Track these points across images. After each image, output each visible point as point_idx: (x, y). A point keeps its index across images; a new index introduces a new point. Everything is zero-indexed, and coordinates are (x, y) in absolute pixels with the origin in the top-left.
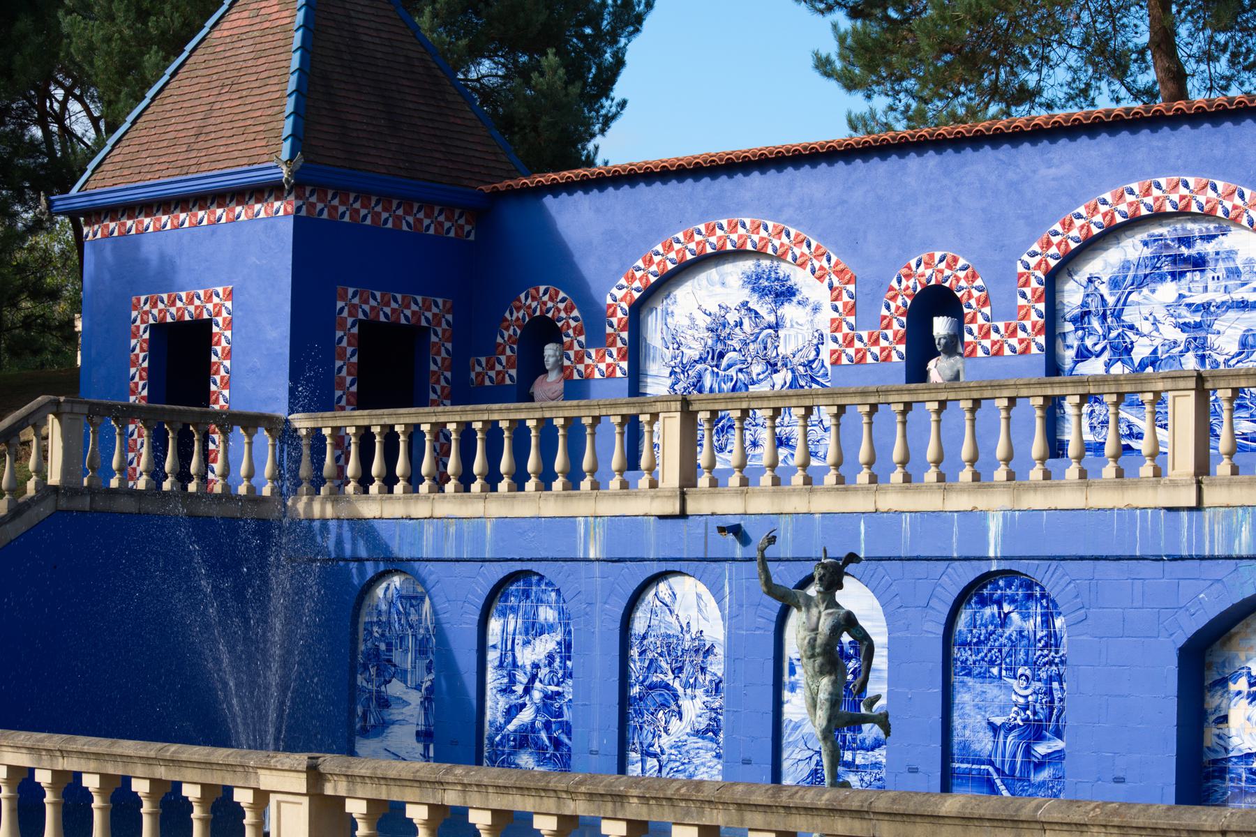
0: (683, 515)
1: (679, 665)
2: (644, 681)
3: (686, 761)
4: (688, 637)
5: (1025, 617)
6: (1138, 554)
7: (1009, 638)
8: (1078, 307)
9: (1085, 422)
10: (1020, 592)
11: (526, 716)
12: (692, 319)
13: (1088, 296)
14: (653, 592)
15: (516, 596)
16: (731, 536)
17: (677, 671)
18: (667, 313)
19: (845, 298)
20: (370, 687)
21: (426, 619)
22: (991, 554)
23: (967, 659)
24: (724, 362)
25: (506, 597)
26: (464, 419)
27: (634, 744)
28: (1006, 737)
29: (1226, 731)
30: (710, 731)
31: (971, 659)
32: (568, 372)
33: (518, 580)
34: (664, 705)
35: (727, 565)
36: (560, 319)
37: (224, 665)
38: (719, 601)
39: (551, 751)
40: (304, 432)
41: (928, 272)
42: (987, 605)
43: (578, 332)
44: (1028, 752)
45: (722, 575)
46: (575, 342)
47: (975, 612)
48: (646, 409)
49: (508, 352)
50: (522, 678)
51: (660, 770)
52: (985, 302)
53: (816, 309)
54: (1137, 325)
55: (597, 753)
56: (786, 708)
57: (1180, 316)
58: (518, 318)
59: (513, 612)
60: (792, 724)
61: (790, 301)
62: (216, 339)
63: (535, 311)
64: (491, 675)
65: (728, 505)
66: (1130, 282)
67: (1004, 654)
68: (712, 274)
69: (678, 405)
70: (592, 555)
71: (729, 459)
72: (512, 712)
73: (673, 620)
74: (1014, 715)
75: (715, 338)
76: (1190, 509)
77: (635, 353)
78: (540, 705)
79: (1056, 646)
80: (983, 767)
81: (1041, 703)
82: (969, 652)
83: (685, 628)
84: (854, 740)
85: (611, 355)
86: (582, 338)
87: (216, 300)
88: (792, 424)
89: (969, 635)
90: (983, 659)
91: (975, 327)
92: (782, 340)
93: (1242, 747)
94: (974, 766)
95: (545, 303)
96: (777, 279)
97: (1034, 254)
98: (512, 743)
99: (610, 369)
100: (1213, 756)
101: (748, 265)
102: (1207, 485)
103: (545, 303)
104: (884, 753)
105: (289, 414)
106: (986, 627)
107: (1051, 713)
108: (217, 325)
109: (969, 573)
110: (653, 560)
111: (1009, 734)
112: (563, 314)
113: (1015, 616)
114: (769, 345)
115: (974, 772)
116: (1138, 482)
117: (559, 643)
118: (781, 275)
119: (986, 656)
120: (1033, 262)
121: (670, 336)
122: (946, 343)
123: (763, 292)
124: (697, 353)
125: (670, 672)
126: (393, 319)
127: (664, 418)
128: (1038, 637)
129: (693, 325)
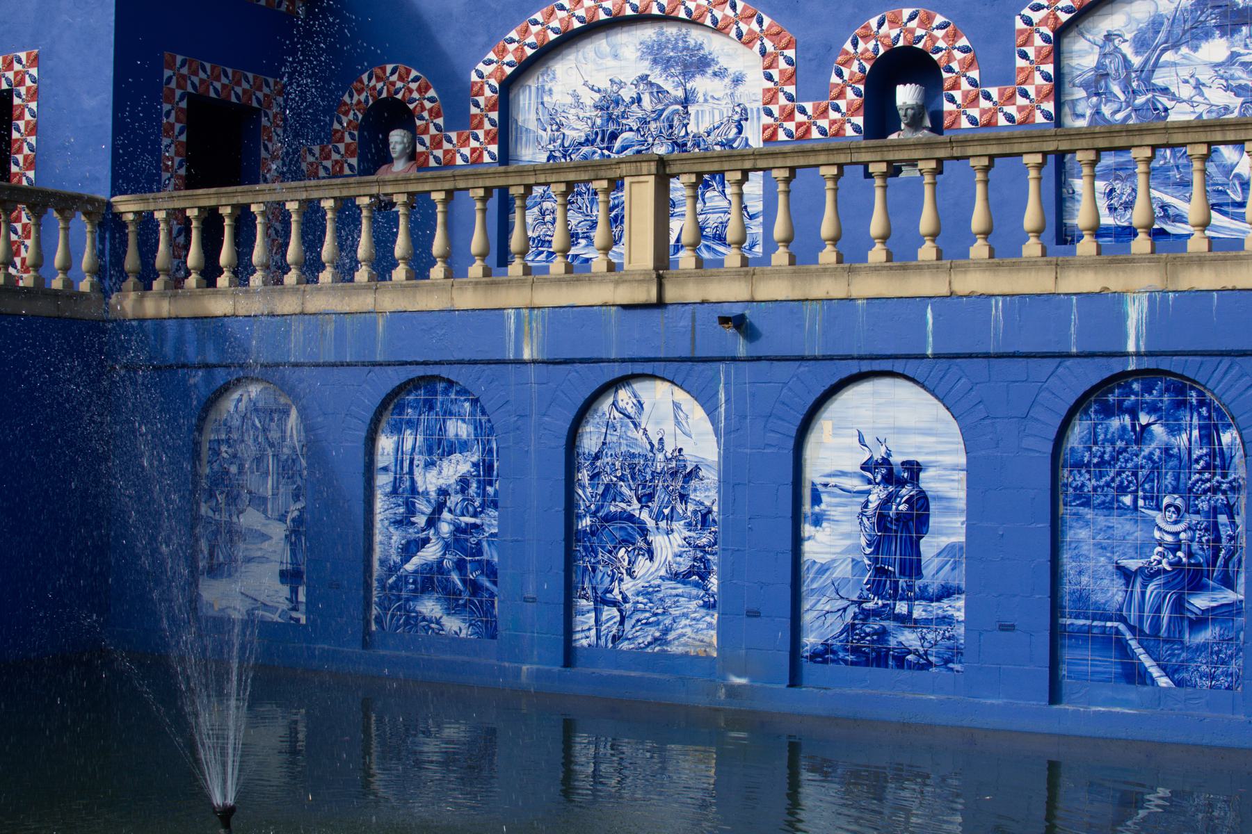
0: (660, 304)
1: (648, 491)
2: (597, 511)
3: (660, 611)
4: (660, 456)
5: (1174, 430)
7: (1149, 458)
8: (1092, 69)
9: (1102, 204)
10: (1166, 398)
11: (431, 553)
12: (576, 96)
13: (1105, 55)
14: (611, 400)
15: (414, 408)
16: (731, 331)
17: (646, 499)
18: (541, 90)
19: (782, 64)
20: (217, 517)
21: (291, 436)
22: (1131, 347)
23: (1083, 485)
24: (618, 144)
25: (400, 409)
26: (345, 193)
27: (583, 589)
28: (1144, 586)
30: (697, 573)
31: (1090, 485)
32: (422, 159)
33: (417, 388)
34: (627, 541)
35: (722, 366)
36: (413, 101)
38: (711, 412)
39: (466, 596)
40: (130, 217)
41: (855, 67)
42: (1113, 415)
43: (435, 113)
45: (714, 380)
46: (431, 125)
47: (1096, 425)
48: (602, 174)
49: (348, 139)
50: (424, 507)
51: (622, 622)
53: (737, 81)
54: (1173, 89)
55: (534, 600)
56: (807, 547)
57: (1232, 77)
58: (359, 102)
59: (410, 427)
60: (816, 567)
61: (703, 73)
62: (17, 113)
63: (380, 92)
64: (380, 504)
65: (729, 292)
66: (1163, 39)
67: (1141, 479)
68: (600, 44)
69: (653, 167)
70: (527, 356)
72: (410, 549)
73: (639, 435)
74: (1158, 558)
75: (606, 117)
77: (505, 134)
78: (450, 540)
79: (1223, 468)
80: (1109, 624)
81: (1200, 542)
82: (1087, 476)
83: (656, 446)
84: (910, 588)
85: (477, 138)
86: (440, 121)
87: (17, 67)
89: (1087, 454)
90: (1108, 485)
91: (957, 95)
92: (692, 117)
94: (1095, 623)
95: (393, 84)
96: (686, 48)
97: (490, 62)
98: (411, 586)
99: (475, 155)
101: (648, 33)
103: (393, 84)
104: (961, 603)
105: (113, 196)
106: (1113, 443)
107: (1216, 556)
108: (19, 96)
109: (1093, 373)
110: (614, 361)
111: (1150, 581)
112: (416, 95)
113: (1158, 429)
114: (676, 123)
115: (1095, 631)
116: (592, 279)
117: (475, 465)
118: (692, 43)
119: (1113, 480)
121: (547, 117)
122: (914, 115)
123: (667, 64)
124: (583, 134)
125: (635, 501)
126: (223, 96)
127: (631, 183)
128: (1194, 456)
129: (579, 104)
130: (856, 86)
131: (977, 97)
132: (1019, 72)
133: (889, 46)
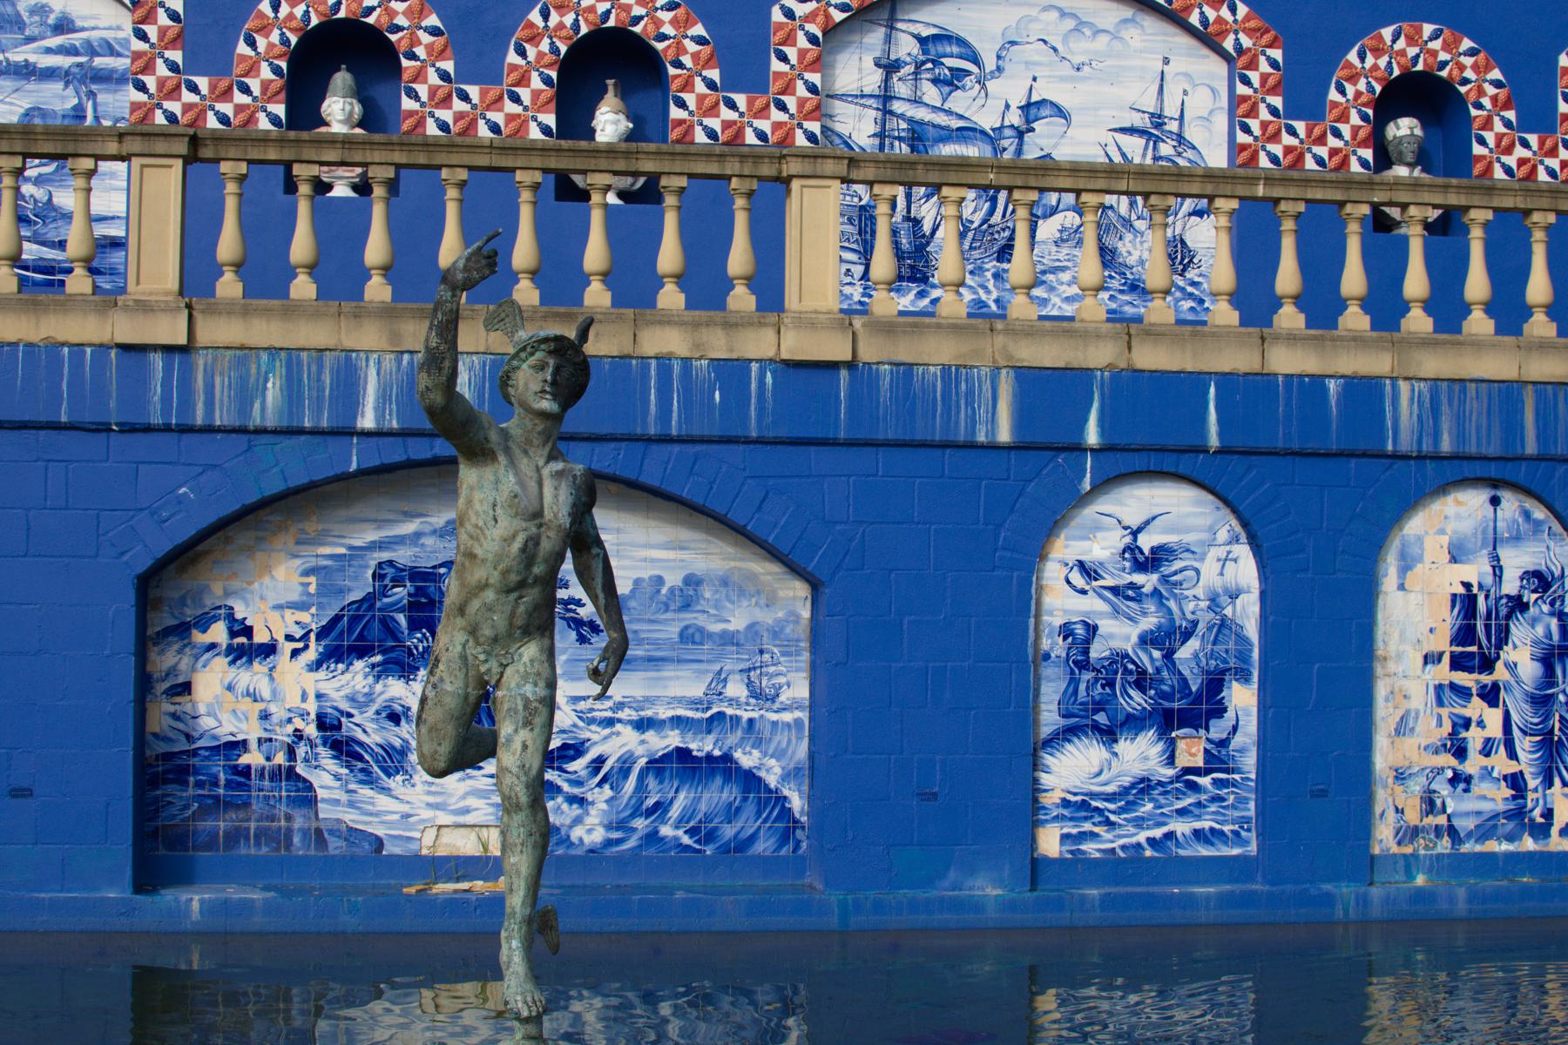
6: (64, 419)
29: (188, 708)
37: (780, 614)
76: (169, 349)
93: (218, 731)
100: (163, 748)
102: (203, 312)
116: (71, 304)
130: (276, 62)
131: (178, 87)
132: (775, 80)
133: (325, 15)
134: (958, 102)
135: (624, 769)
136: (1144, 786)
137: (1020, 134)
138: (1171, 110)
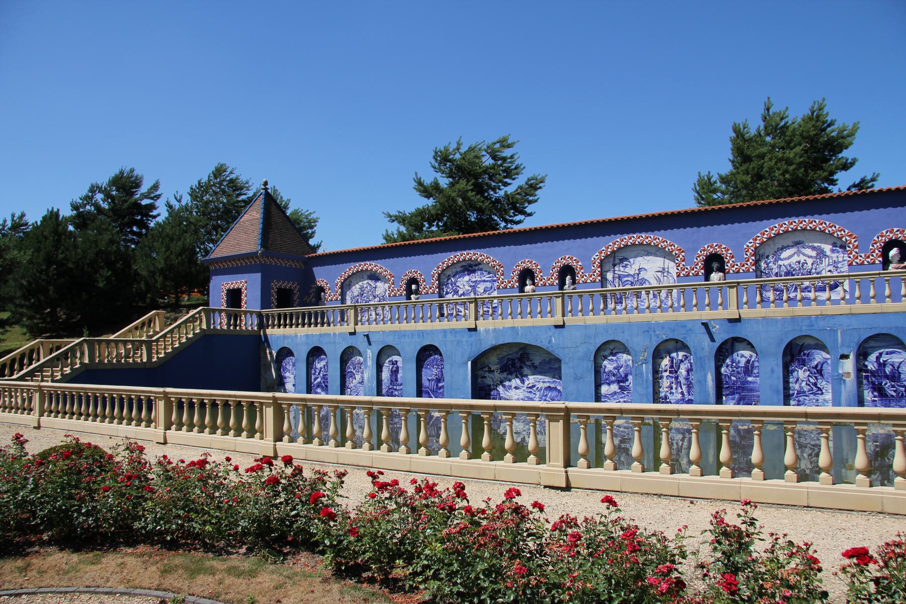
11: (319, 380)
17: (354, 369)
44: (437, 385)
50: (318, 371)
52: (424, 281)
71: (364, 319)
72: (316, 379)
88: (380, 310)
91: (729, 265)
97: (750, 243)
120: (750, 245)
134: (627, 270)
135: (541, 388)
136: (615, 393)
137: (638, 274)
138: (666, 267)
